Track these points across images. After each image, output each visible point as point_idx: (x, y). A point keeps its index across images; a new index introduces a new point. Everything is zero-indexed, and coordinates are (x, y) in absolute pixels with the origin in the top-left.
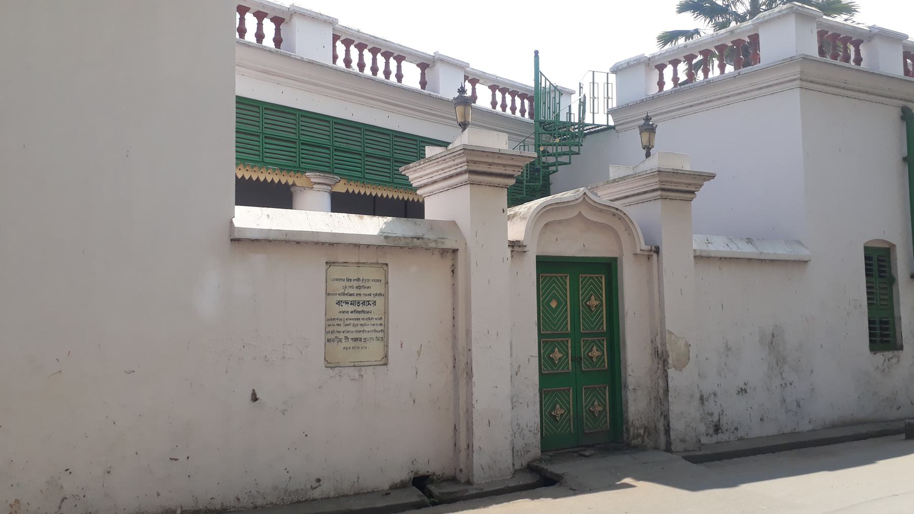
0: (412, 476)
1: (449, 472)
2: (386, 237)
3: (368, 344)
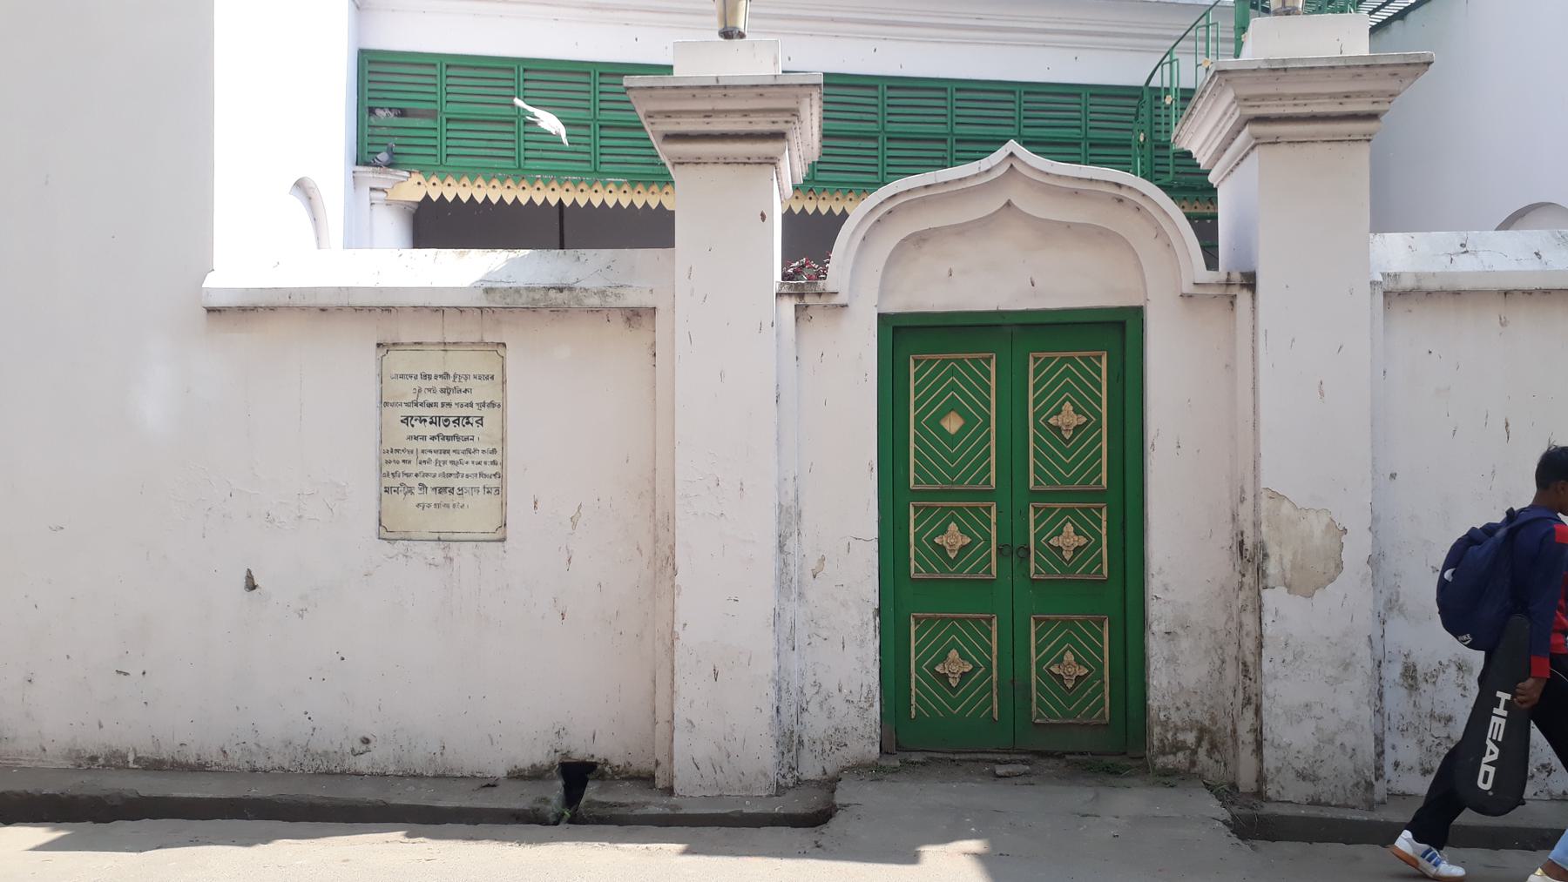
0: (557, 759)
1: (640, 763)
2: (487, 291)
3: (467, 499)
